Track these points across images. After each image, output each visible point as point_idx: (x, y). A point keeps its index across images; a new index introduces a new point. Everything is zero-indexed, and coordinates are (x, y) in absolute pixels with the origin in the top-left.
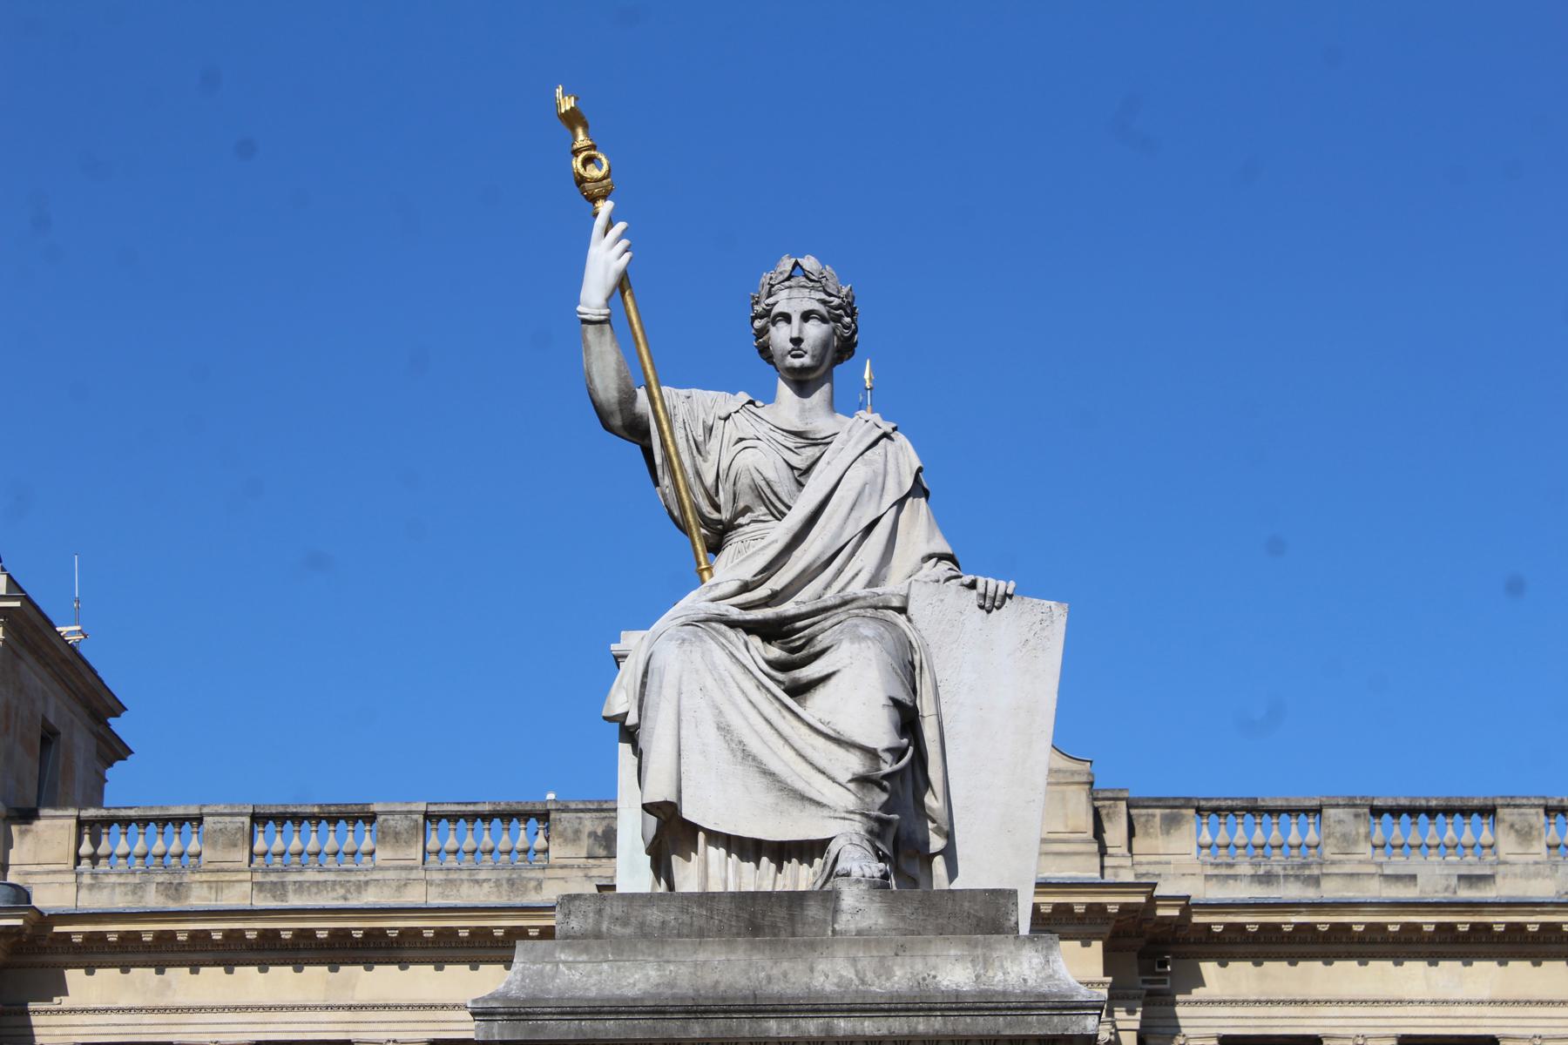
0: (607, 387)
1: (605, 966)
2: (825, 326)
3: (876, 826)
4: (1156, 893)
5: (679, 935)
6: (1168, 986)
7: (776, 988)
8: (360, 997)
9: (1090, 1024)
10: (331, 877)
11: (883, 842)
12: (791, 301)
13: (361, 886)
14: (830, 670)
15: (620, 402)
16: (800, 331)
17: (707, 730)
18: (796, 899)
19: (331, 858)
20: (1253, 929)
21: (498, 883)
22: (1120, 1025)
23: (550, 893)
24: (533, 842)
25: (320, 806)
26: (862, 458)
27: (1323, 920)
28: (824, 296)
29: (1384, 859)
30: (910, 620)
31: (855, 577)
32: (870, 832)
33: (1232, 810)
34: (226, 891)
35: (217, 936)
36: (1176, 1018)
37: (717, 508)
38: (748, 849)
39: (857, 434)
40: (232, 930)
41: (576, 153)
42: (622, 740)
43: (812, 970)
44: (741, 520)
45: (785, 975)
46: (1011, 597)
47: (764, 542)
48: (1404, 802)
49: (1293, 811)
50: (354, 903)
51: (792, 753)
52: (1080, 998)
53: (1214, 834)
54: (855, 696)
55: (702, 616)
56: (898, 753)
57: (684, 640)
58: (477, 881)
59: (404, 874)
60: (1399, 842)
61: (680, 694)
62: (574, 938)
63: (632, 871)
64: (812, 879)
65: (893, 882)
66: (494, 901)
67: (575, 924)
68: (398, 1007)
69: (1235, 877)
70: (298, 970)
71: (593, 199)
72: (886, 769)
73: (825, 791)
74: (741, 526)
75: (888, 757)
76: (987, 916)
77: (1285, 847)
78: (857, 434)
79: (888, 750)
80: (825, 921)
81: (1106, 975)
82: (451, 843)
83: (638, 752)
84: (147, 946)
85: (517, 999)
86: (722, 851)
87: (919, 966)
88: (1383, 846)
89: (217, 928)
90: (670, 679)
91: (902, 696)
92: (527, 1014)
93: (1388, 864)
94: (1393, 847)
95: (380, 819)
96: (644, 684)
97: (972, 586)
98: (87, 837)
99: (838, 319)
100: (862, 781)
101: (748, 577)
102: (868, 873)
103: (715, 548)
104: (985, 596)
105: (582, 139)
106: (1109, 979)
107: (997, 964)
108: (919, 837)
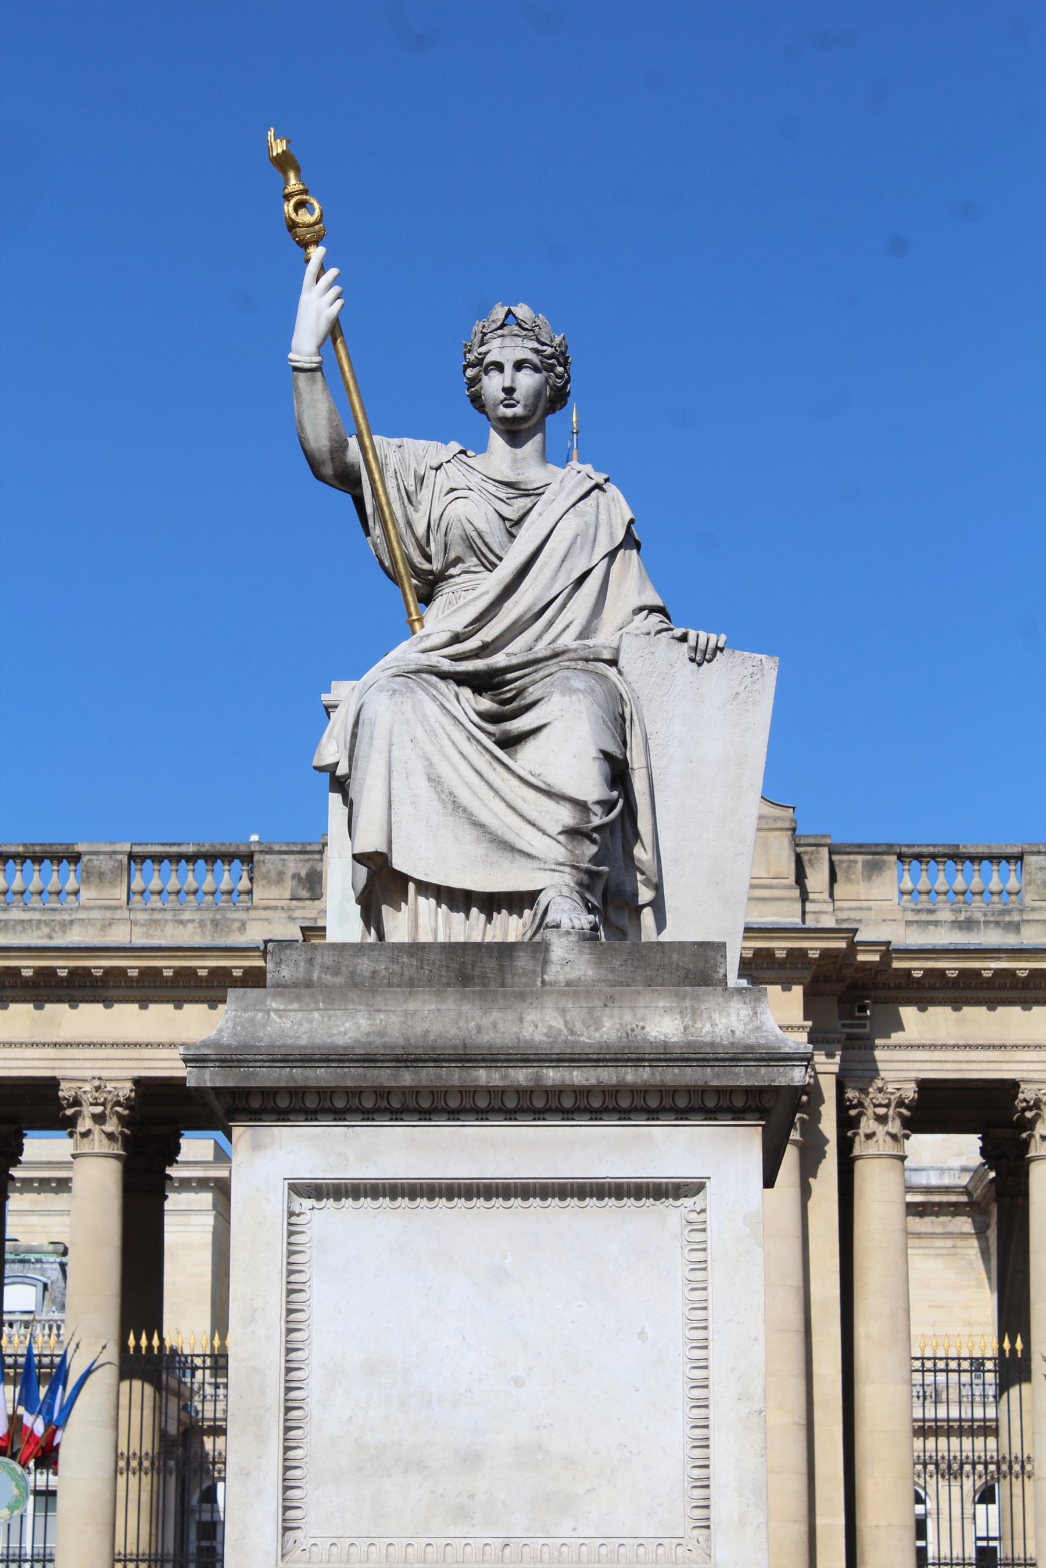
0: (319, 438)
1: (316, 1015)
2: (538, 376)
3: (585, 878)
4: (857, 938)
5: (389, 985)
6: (867, 1030)
7: (486, 1038)
9: (798, 1076)
10: (36, 916)
11: (593, 894)
12: (505, 349)
14: (541, 723)
15: (332, 451)
16: (513, 380)
17: (422, 785)
18: (505, 950)
19: (36, 898)
20: (952, 974)
21: (202, 924)
22: (819, 1068)
23: (255, 934)
25: (25, 845)
26: (574, 509)
30: (620, 673)
31: (566, 629)
32: (580, 884)
33: (933, 857)
36: (875, 1061)
37: (428, 558)
38: (459, 900)
39: (569, 485)
41: (287, 197)
43: (521, 1020)
44: (452, 571)
45: (495, 1025)
46: (722, 650)
47: (472, 595)
50: (59, 941)
51: (503, 805)
52: (787, 1050)
53: (915, 880)
55: (413, 667)
56: (608, 805)
57: (395, 692)
58: (181, 922)
59: (108, 914)
61: (391, 745)
62: (285, 986)
63: (343, 923)
64: (521, 930)
66: (198, 941)
67: (286, 973)
68: (102, 1045)
69: (936, 923)
71: (305, 245)
72: (596, 821)
73: (535, 843)
74: (452, 576)
76: (694, 969)
77: (951, 893)
78: (569, 485)
79: (599, 803)
80: (534, 972)
81: (806, 1018)
82: (155, 884)
83: (348, 803)
85: (229, 1047)
86: (432, 901)
90: (381, 730)
91: (613, 749)
92: (239, 1061)
95: (85, 859)
96: (354, 735)
97: (683, 639)
98: (217, 1336)
99: (551, 368)
100: (572, 833)
101: (459, 628)
102: (577, 924)
103: (426, 598)
104: (695, 649)
105: (293, 183)
106: (809, 1023)
107: (705, 1015)
108: (629, 888)
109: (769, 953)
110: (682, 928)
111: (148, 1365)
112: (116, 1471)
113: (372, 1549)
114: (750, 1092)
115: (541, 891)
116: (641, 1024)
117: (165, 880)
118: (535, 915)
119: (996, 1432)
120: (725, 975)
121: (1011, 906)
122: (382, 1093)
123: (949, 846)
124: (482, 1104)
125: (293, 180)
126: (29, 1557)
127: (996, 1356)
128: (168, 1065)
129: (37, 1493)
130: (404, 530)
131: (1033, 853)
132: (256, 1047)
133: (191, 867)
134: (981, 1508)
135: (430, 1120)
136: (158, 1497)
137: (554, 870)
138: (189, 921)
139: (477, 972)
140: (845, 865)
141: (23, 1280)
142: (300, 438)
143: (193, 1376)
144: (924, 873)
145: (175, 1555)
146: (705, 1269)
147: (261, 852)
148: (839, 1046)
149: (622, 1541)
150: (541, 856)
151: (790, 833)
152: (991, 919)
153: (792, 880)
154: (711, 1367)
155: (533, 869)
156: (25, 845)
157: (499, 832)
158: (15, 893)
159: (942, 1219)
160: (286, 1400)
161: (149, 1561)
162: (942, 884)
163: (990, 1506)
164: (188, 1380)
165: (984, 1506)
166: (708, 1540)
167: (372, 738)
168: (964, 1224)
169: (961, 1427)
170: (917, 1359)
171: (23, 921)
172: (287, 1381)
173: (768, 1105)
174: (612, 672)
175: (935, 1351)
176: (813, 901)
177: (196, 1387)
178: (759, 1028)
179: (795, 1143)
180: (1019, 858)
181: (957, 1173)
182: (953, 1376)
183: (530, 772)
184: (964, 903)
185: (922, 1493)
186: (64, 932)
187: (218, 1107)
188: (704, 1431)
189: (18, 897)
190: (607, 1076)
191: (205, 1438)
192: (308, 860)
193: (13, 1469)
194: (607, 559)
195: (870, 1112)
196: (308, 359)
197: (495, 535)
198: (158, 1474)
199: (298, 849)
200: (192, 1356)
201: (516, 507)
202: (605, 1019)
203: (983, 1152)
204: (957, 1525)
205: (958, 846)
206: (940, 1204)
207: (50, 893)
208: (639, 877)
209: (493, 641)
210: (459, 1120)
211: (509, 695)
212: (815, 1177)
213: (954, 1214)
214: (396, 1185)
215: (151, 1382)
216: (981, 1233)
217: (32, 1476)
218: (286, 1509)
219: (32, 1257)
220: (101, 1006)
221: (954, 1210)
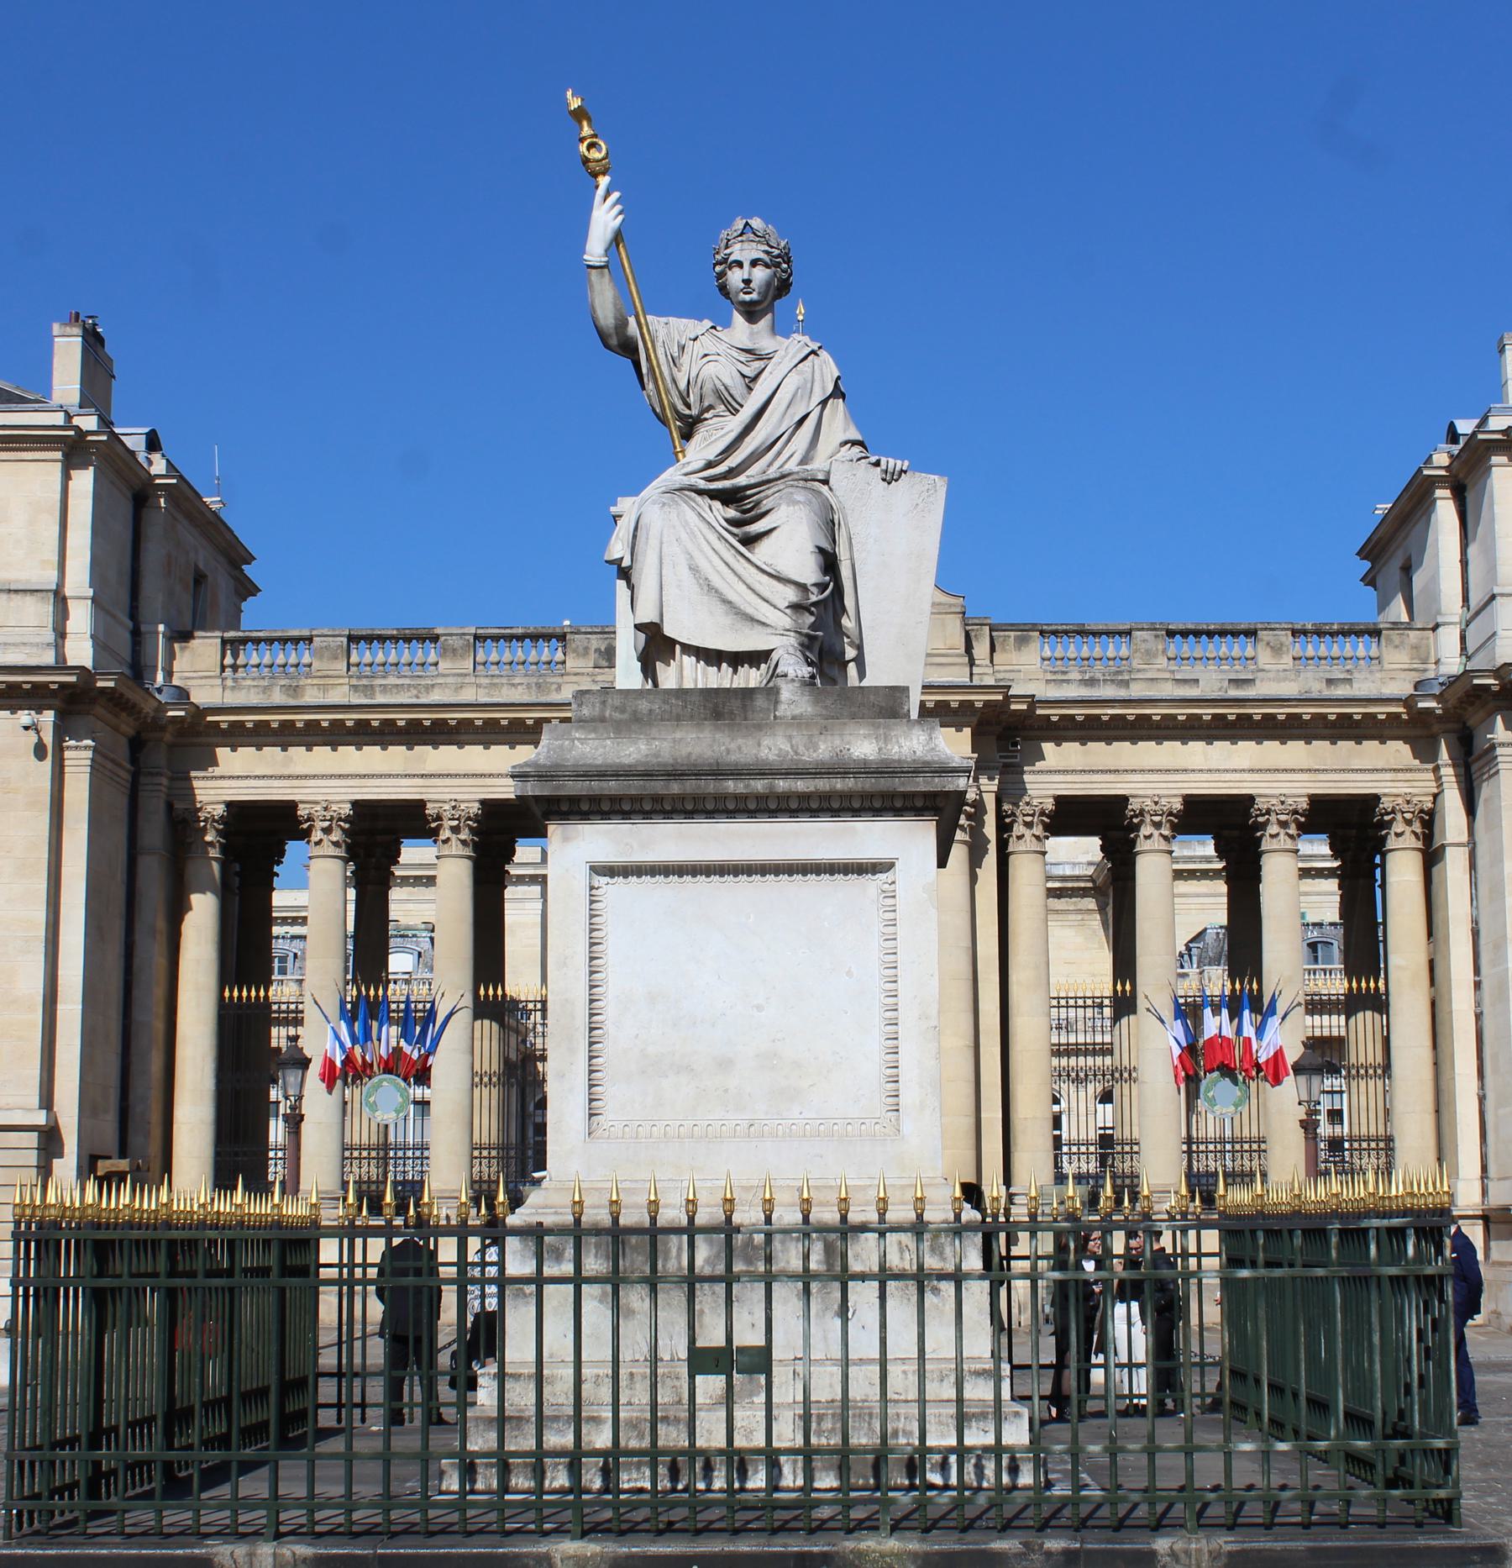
0: (607, 317)
9: (961, 783)
10: (407, 681)
12: (743, 251)
13: (429, 688)
15: (616, 328)
17: (685, 573)
18: (747, 693)
21: (529, 686)
27: (1131, 712)
31: (790, 457)
32: (802, 645)
33: (1066, 632)
37: (688, 406)
39: (792, 351)
41: (582, 140)
44: (706, 415)
45: (740, 748)
48: (1190, 626)
49: (1109, 633)
53: (1053, 650)
54: (790, 545)
56: (822, 587)
59: (460, 680)
63: (627, 674)
65: (818, 681)
66: (526, 699)
69: (1068, 681)
71: (595, 175)
72: (814, 598)
76: (887, 706)
78: (792, 351)
82: (494, 657)
83: (631, 587)
89: (325, 718)
96: (635, 537)
97: (877, 464)
99: (778, 265)
100: (796, 607)
101: (712, 458)
102: (800, 674)
103: (687, 436)
104: (886, 472)
105: (586, 130)
110: (879, 674)
111: (494, 1008)
114: (927, 795)
117: (501, 654)
119: (1111, 1052)
122: (657, 799)
124: (731, 806)
128: (506, 790)
129: (416, 1103)
134: (1100, 1107)
136: (504, 1104)
141: (403, 950)
166: (898, 1119)
168: (1090, 903)
180: (1128, 633)
182: (1080, 1011)
187: (537, 810)
190: (822, 784)
195: (1020, 819)
197: (737, 387)
203: (1103, 848)
204: (1083, 1119)
206: (1072, 889)
216: (1102, 909)
218: (591, 1100)
219: (410, 933)
221: (1083, 893)
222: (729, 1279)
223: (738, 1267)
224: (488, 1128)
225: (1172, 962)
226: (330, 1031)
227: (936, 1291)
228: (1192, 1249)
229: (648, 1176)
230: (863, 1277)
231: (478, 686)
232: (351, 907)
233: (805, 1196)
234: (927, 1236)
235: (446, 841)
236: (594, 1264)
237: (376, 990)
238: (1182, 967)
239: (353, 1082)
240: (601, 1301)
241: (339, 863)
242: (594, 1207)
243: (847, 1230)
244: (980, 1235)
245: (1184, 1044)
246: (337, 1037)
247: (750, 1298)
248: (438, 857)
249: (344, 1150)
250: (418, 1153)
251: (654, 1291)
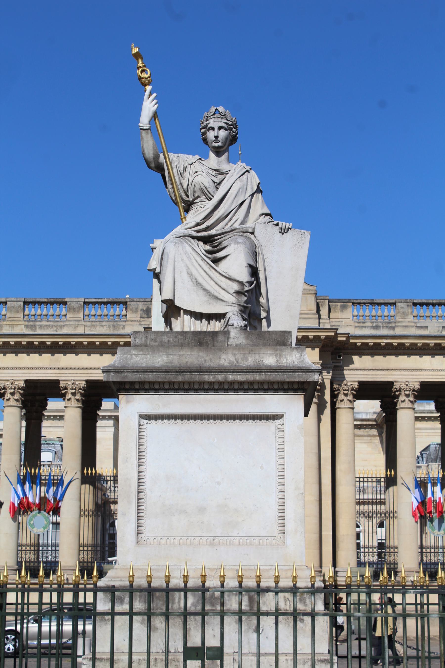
0: (149, 153)
1: (148, 356)
2: (226, 132)
3: (242, 308)
4: (338, 332)
5: (174, 346)
6: (341, 364)
8: (62, 365)
9: (316, 377)
11: (245, 314)
12: (214, 123)
13: (62, 327)
15: (154, 158)
16: (218, 133)
17: (186, 277)
18: (214, 334)
19: (51, 317)
21: (109, 326)
22: (324, 377)
23: (128, 330)
24: (121, 312)
25: (47, 299)
26: (239, 179)
27: (395, 342)
28: (226, 121)
29: (417, 321)
30: (255, 237)
31: (236, 221)
32: (241, 311)
33: (365, 303)
34: (15, 328)
35: (12, 343)
36: (344, 375)
37: (188, 196)
39: (237, 170)
40: (17, 341)
41: (138, 68)
42: (154, 278)
43: (220, 358)
44: (196, 201)
45: (211, 359)
46: (291, 229)
48: (424, 301)
49: (386, 304)
50: (59, 332)
51: (214, 283)
52: (312, 369)
53: (358, 312)
54: (236, 263)
55: (182, 234)
56: (251, 283)
58: (102, 326)
59: (77, 323)
60: (422, 315)
61: (175, 262)
62: (138, 346)
63: (158, 323)
64: (220, 327)
65: (248, 328)
66: (108, 332)
67: (138, 341)
68: (75, 368)
69: (365, 327)
70: (40, 355)
71: (144, 85)
72: (246, 289)
73: (225, 296)
74: (196, 203)
75: (247, 284)
76: (281, 340)
77: (371, 316)
78: (237, 170)
79: (247, 282)
80: (225, 341)
81: (320, 360)
82: (93, 312)
83: (160, 282)
84: (12, 346)
85: (118, 367)
86: (189, 317)
87: (257, 357)
88: (417, 316)
89: (12, 340)
90: (171, 256)
91: (252, 263)
92: (121, 372)
93: (418, 322)
94: (420, 317)
95: (68, 303)
96: (162, 258)
97: (277, 225)
99: (231, 129)
100: (238, 293)
101: (198, 221)
102: (240, 325)
103: (187, 210)
104: (281, 228)
105: (141, 63)
106: (321, 361)
107: (284, 356)
108: (258, 312)
109: (307, 337)
111: (91, 479)
112: (80, 516)
113: (168, 540)
115: (227, 313)
116: (262, 359)
117: (96, 311)
118: (225, 321)
119: (384, 503)
120: (291, 343)
121: (392, 321)
122: (171, 383)
123: (370, 300)
125: (140, 62)
126: (50, 545)
127: (385, 476)
128: (99, 376)
129: (53, 523)
130: (179, 186)
131: (399, 302)
132: (127, 367)
133: (105, 306)
134: (379, 529)
135: (188, 393)
137: (232, 306)
138: (105, 325)
139: (205, 341)
140: (334, 306)
141: (48, 450)
142: (143, 153)
143: (107, 483)
144: (361, 309)
145: (101, 544)
146: (284, 444)
147: (130, 301)
148: (331, 369)
149: (254, 538)
150: (227, 301)
151: (315, 295)
152: (385, 325)
153: (315, 311)
154: (285, 478)
155: (224, 305)
156: (47, 299)
157: (212, 292)
158: (44, 316)
159: (367, 430)
160: (138, 489)
161: (92, 546)
162: (367, 313)
163: (382, 529)
164: (105, 485)
165: (380, 529)
166: (284, 537)
167: (168, 259)
168: (375, 432)
169: (372, 502)
170: (357, 478)
171: (47, 325)
172: (138, 483)
173: (306, 388)
174: (252, 236)
175: (364, 475)
176: (323, 319)
177: (108, 487)
178: (303, 361)
179: (315, 403)
180: (394, 304)
181: (372, 414)
182: (370, 484)
183: (223, 272)
184: (375, 320)
185: (359, 524)
186: (61, 329)
187: (114, 388)
188: (283, 500)
189: (45, 317)
191: (111, 505)
192: (146, 304)
193: (45, 515)
194: (250, 197)
195: (342, 392)
196: (146, 126)
197: (211, 188)
198: (95, 516)
199: (143, 300)
200: (106, 476)
201: (219, 178)
202: (249, 358)
203: (381, 406)
204: (371, 535)
205: (373, 300)
206: (366, 425)
207: (56, 315)
208: (261, 308)
209: (211, 225)
210: (198, 393)
211: (216, 244)
212: (323, 415)
213: (371, 428)
214: (176, 415)
215: (92, 485)
216: (380, 435)
217: (51, 518)
218: (138, 526)
219: (51, 442)
220: (74, 355)
221: (371, 427)
222: (203, 614)
223: (208, 607)
224: (87, 536)
225: (414, 461)
226: (12, 489)
227: (302, 620)
228: (425, 602)
229: (165, 563)
230: (267, 614)
231: (85, 326)
232: (24, 430)
233: (240, 574)
234: (298, 594)
235: (69, 400)
236: (139, 606)
237: (35, 470)
238: (418, 463)
239: (23, 514)
240: (141, 623)
241: (18, 409)
242: (139, 578)
243: (260, 591)
244: (323, 594)
245: (420, 501)
246: (16, 492)
247: (213, 622)
248: (65, 407)
249: (18, 546)
250: (54, 548)
251: (167, 619)
